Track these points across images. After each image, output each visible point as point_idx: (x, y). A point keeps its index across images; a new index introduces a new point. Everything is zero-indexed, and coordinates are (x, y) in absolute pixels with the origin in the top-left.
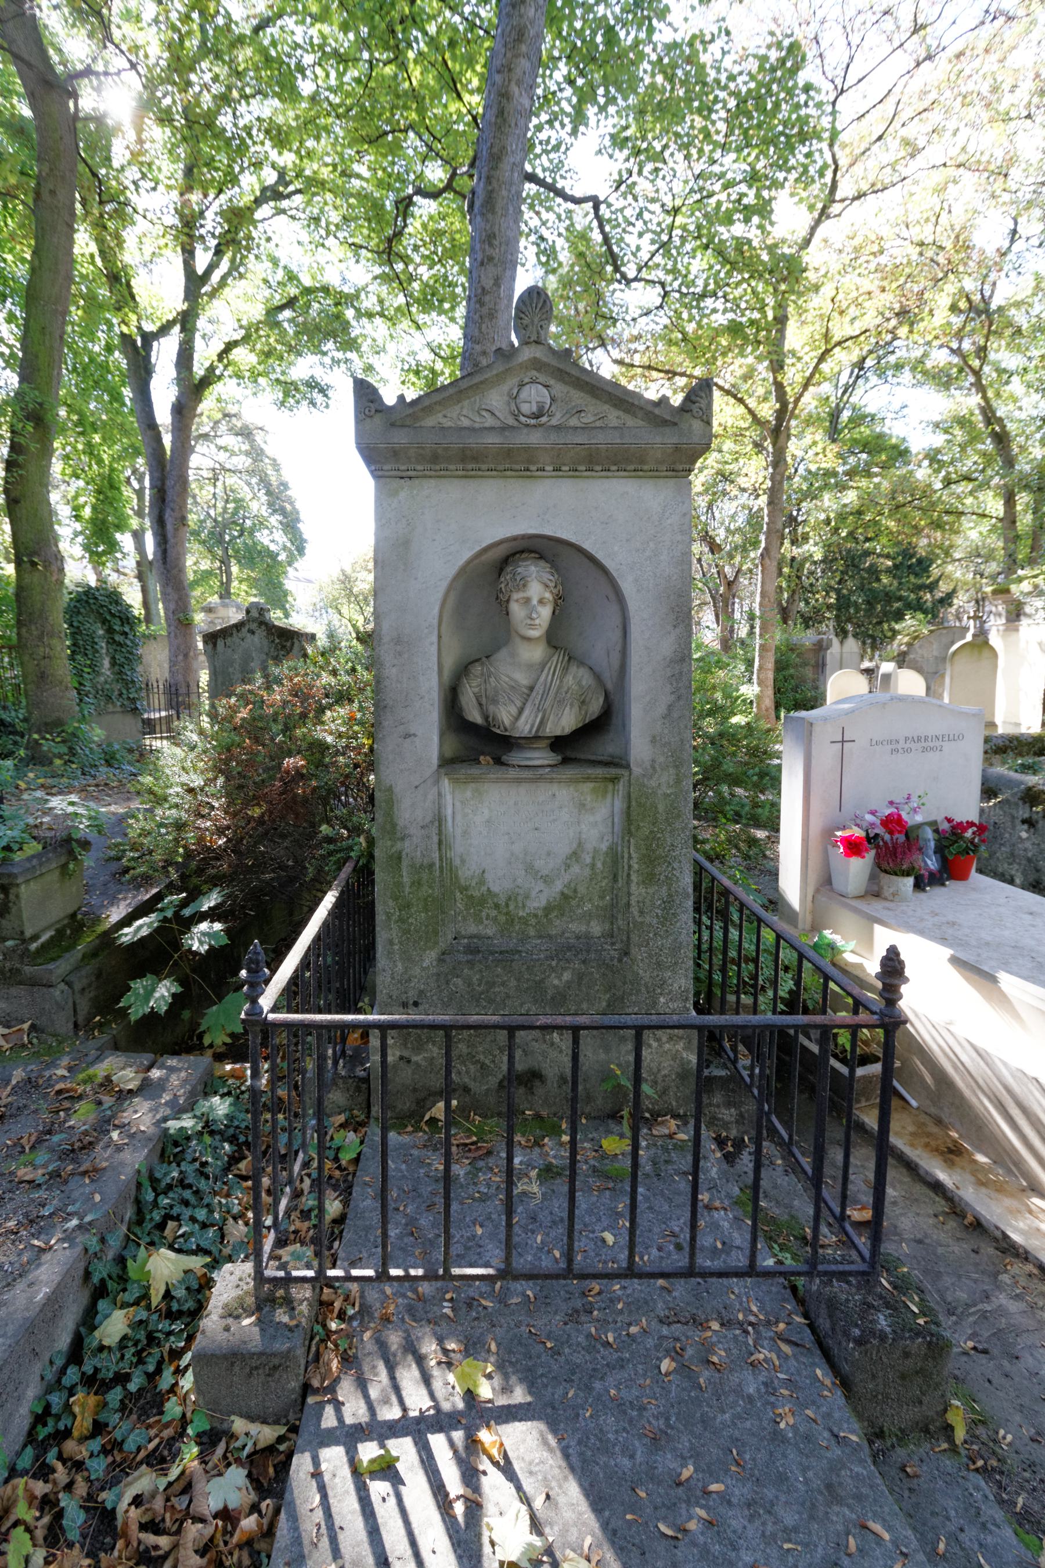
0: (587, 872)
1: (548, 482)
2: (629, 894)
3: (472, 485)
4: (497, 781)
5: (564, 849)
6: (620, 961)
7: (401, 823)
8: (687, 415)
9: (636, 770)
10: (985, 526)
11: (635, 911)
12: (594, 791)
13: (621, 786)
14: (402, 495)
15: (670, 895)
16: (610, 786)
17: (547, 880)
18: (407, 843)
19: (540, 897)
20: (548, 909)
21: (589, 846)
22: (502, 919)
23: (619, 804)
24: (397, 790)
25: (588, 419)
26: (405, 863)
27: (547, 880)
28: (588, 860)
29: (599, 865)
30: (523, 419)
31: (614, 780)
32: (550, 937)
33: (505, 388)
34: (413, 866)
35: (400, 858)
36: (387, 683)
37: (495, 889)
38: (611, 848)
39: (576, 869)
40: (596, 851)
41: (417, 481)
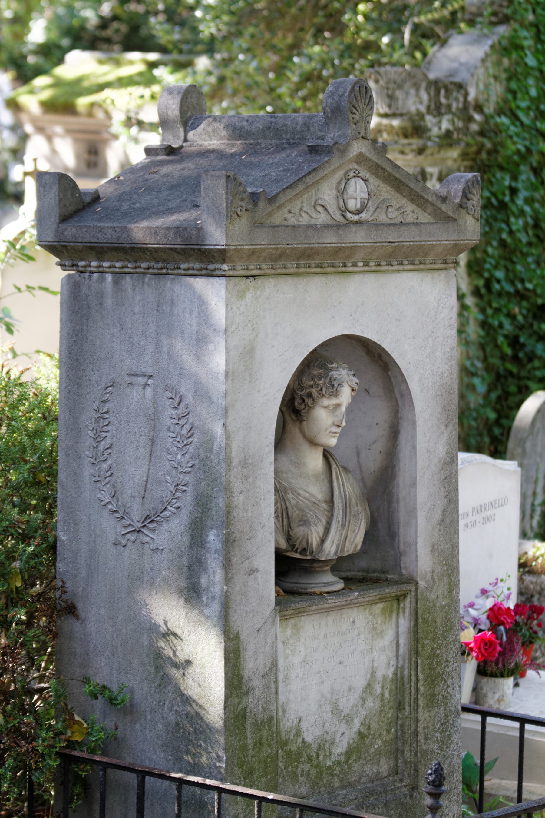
0: (378, 703)
1: (358, 278)
2: (417, 720)
3: (302, 282)
5: (360, 683)
6: (411, 796)
7: (246, 674)
8: (463, 212)
9: (422, 584)
10: (308, 51)
11: (421, 738)
13: (407, 603)
14: (249, 296)
15: (446, 716)
17: (348, 720)
18: (251, 698)
19: (343, 738)
20: (348, 754)
21: (379, 675)
22: (314, 772)
23: (404, 623)
24: (243, 637)
25: (393, 214)
26: (249, 722)
27: (348, 720)
28: (379, 691)
29: (387, 695)
30: (349, 215)
31: (399, 599)
32: (350, 785)
33: (334, 181)
34: (254, 724)
35: (245, 717)
36: (235, 513)
37: (309, 738)
38: (395, 674)
39: (370, 703)
40: (385, 678)
41: (259, 281)
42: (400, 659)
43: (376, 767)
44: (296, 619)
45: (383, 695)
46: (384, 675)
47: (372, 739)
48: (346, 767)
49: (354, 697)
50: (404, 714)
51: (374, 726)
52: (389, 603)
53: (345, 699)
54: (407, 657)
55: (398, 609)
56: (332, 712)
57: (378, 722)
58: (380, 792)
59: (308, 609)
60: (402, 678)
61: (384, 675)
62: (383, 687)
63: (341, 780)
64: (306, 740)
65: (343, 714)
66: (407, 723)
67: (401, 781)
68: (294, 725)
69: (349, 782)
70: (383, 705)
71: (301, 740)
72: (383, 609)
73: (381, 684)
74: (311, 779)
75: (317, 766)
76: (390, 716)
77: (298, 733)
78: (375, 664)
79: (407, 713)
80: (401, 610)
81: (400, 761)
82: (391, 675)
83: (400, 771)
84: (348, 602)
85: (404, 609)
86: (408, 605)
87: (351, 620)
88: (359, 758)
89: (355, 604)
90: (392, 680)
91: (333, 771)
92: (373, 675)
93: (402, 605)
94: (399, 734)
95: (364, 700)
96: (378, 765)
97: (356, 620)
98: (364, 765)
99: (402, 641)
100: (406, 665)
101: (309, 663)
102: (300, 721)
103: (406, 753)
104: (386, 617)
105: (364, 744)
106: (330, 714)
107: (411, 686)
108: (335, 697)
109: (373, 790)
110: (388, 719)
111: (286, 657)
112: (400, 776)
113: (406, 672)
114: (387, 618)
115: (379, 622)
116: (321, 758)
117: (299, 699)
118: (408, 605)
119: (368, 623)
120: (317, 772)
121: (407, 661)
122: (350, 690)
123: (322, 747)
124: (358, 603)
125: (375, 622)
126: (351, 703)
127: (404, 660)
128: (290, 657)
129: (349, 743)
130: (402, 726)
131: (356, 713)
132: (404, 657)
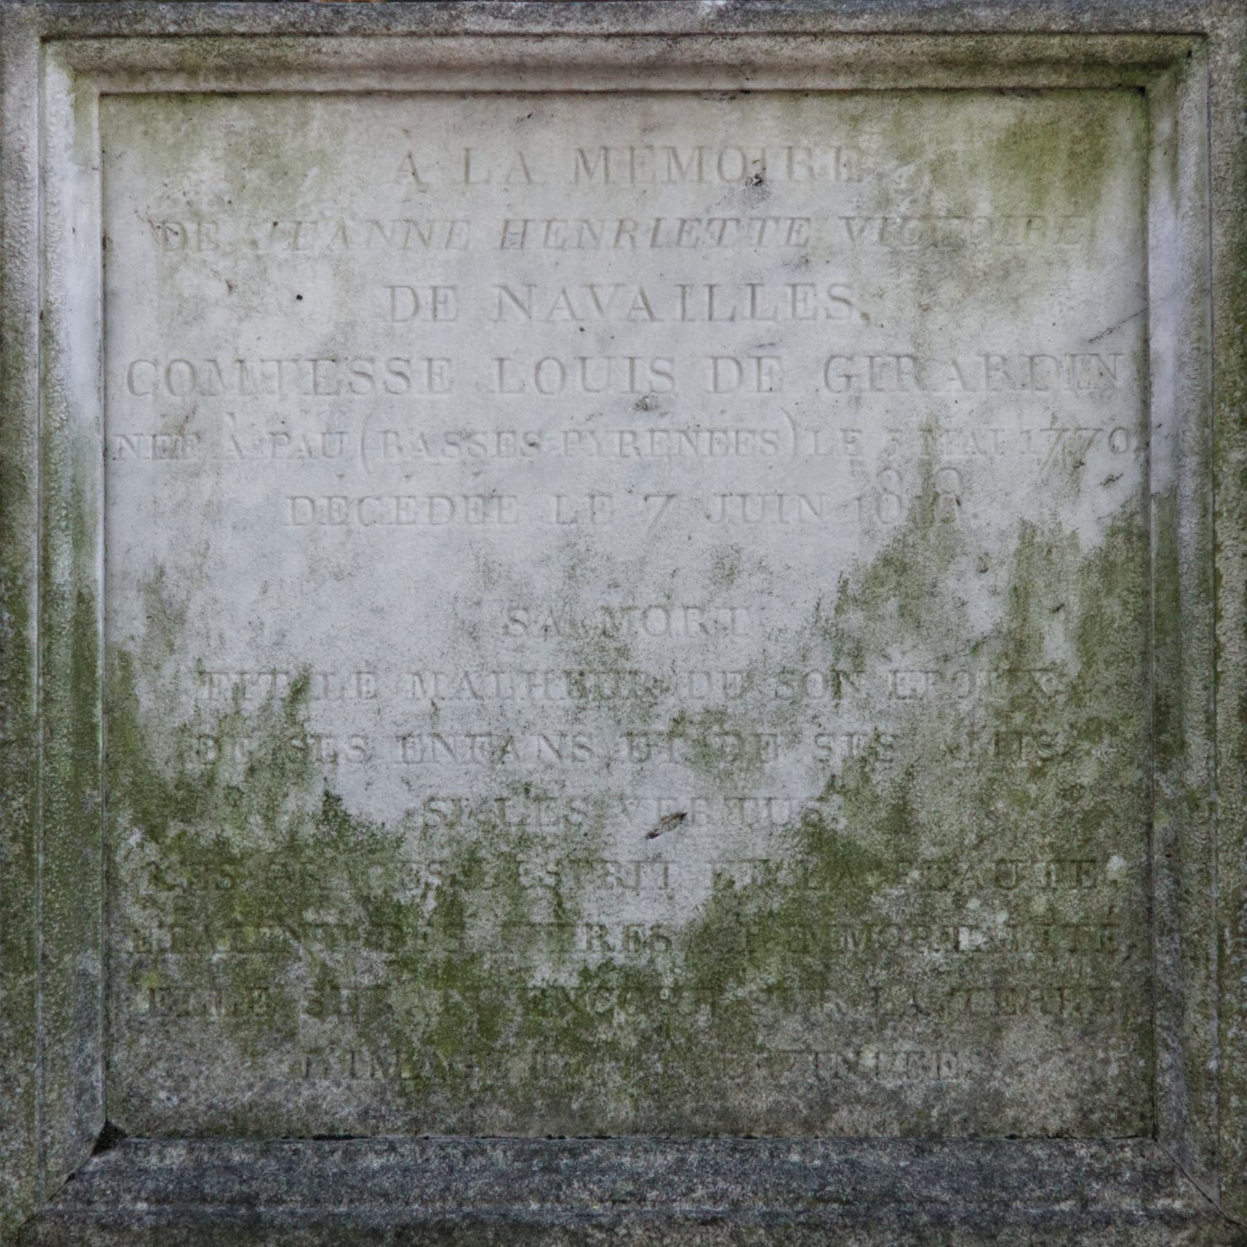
0: (978, 688)
4: (392, 85)
12: (1016, 148)
16: (1123, 123)
20: (721, 944)
21: (989, 519)
22: (421, 1005)
28: (985, 613)
29: (1057, 644)
37: (377, 802)
39: (903, 671)
40: (1035, 548)
42: (1160, 447)
43: (967, 1061)
44: (269, 109)
45: (1016, 651)
46: (1027, 532)
47: (925, 889)
48: (702, 1020)
49: (772, 622)
50: (1181, 783)
51: (945, 812)
52: (1073, 105)
53: (684, 623)
54: (1192, 436)
55: (1147, 147)
56: (577, 681)
57: (984, 801)
58: (940, 1220)
59: (297, 50)
60: (1172, 562)
61: (1027, 532)
62: (1020, 596)
63: (659, 1091)
64: (351, 806)
65: (669, 705)
66: (1197, 838)
67: (1154, 1180)
68: (250, 706)
69: (724, 1114)
70: (1027, 701)
71: (314, 803)
72: (1016, 137)
73: (1002, 577)
74: (398, 1038)
75: (450, 974)
76: (1087, 774)
77: (288, 758)
78: (952, 452)
79: (1194, 778)
80: (1158, 159)
81: (1166, 1058)
82: (1091, 538)
83: (1167, 1120)
84: (653, 49)
85: (1174, 145)
86: (1193, 125)
87: (733, 168)
88: (818, 982)
89: (698, 67)
90: (1106, 567)
91: (586, 1022)
92: (930, 507)
93: (1164, 127)
94: (1160, 893)
95: (851, 656)
96: (989, 1054)
97: (776, 172)
98: (852, 1032)
99: (1164, 341)
100: (1189, 486)
101: (380, 369)
102: (299, 690)
103: (1193, 1017)
104: (1039, 191)
105: (862, 907)
106: (560, 687)
107: (1217, 616)
108: (592, 597)
109: (889, 1195)
110: (1069, 792)
111: (188, 313)
112: (1160, 1154)
113: (1188, 527)
114: (1057, 198)
115: (984, 208)
116: (482, 931)
117: (294, 565)
118: (1193, 125)
119: (884, 201)
120: (449, 1008)
121: (1192, 462)
122: (726, 571)
123: (491, 868)
124: (733, 69)
125: (941, 201)
126: (742, 648)
127: (1177, 456)
128: (218, 318)
129: (722, 883)
130: (1174, 849)
131: (781, 717)
132: (1176, 438)
